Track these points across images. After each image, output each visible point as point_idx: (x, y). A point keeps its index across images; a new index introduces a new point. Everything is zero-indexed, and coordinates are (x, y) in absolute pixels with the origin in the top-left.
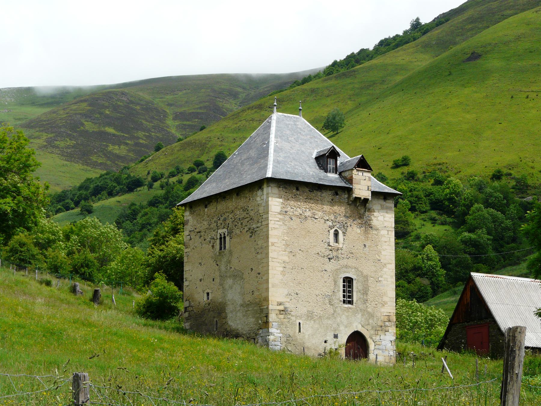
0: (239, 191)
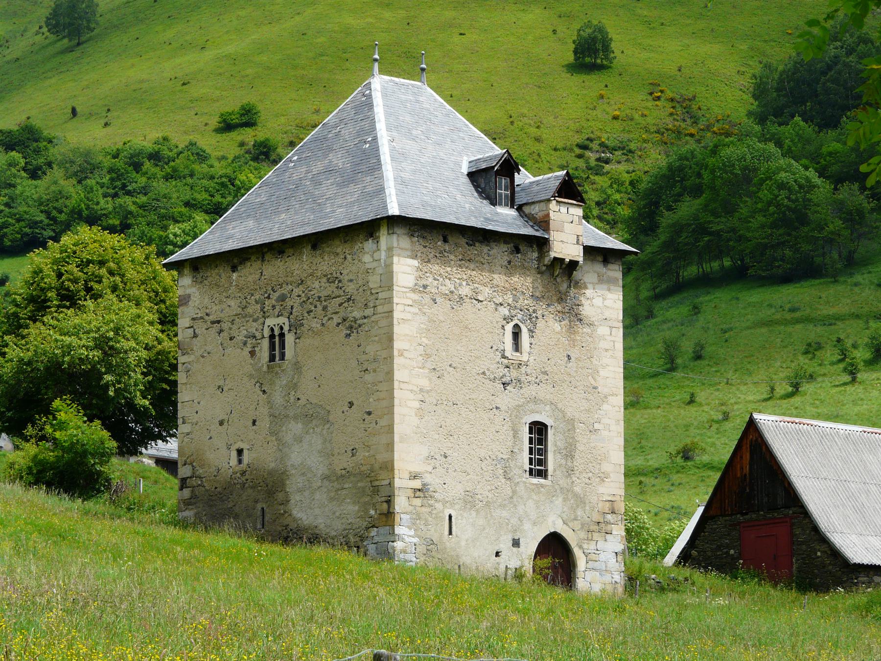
0: (317, 241)
